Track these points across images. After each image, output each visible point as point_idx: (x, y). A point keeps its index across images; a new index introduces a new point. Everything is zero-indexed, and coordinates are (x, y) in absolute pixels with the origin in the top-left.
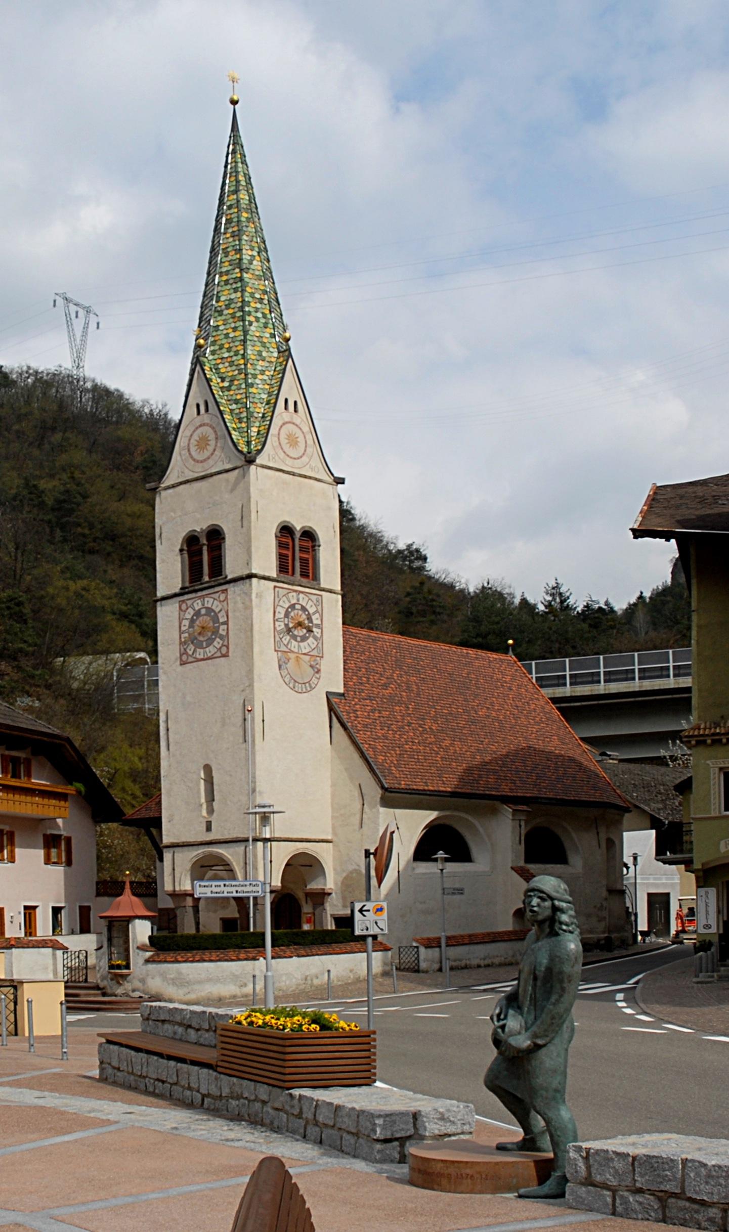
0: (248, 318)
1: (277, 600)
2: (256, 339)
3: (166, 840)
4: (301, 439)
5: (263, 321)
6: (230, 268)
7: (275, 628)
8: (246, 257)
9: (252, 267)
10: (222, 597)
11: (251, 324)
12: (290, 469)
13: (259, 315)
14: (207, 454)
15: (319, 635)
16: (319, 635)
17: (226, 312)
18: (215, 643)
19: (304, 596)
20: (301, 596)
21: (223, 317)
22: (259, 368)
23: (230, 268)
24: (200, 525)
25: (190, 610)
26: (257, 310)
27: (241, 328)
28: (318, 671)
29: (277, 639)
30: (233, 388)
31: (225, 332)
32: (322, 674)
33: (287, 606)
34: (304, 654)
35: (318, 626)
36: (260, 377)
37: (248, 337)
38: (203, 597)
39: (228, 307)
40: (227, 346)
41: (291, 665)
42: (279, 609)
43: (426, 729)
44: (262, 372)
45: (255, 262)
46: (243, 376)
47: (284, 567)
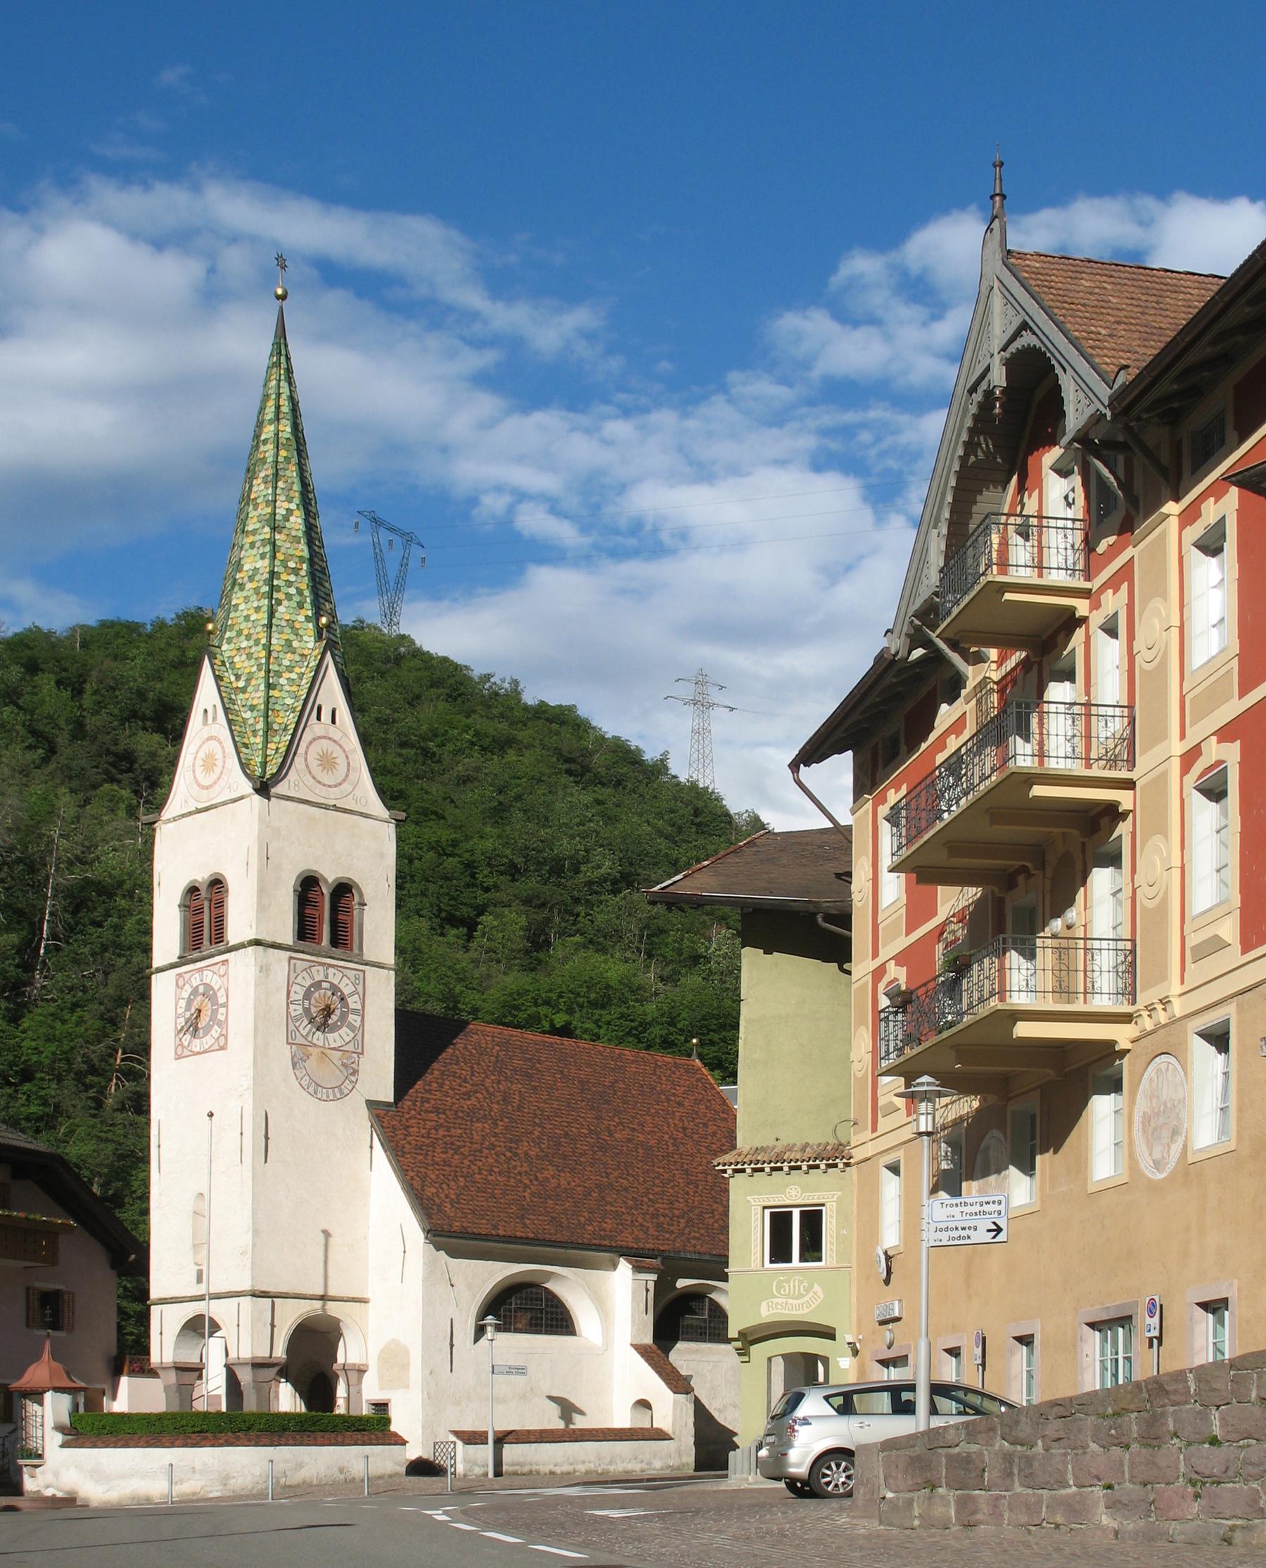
0: (275, 595)
1: (293, 975)
2: (284, 623)
3: (154, 1294)
4: (341, 761)
5: (297, 598)
6: (258, 525)
7: (288, 1013)
8: (281, 512)
9: (287, 524)
10: (223, 969)
11: (279, 602)
12: (321, 801)
13: (292, 591)
14: (214, 776)
15: (357, 1024)
16: (357, 1024)
17: (249, 586)
18: (213, 1032)
19: (339, 974)
20: (331, 971)
21: (245, 593)
22: (286, 663)
23: (258, 525)
24: (202, 876)
25: (187, 986)
26: (289, 584)
27: (265, 608)
28: (355, 1072)
29: (292, 1027)
30: (250, 689)
31: (245, 613)
32: (361, 1076)
33: (308, 983)
34: (334, 1049)
35: (356, 1012)
36: (286, 675)
37: (274, 621)
38: (201, 970)
39: (251, 579)
40: (246, 632)
41: (311, 1063)
42: (295, 988)
43: (516, 1154)
44: (290, 669)
45: (292, 519)
46: (262, 674)
47: (305, 930)
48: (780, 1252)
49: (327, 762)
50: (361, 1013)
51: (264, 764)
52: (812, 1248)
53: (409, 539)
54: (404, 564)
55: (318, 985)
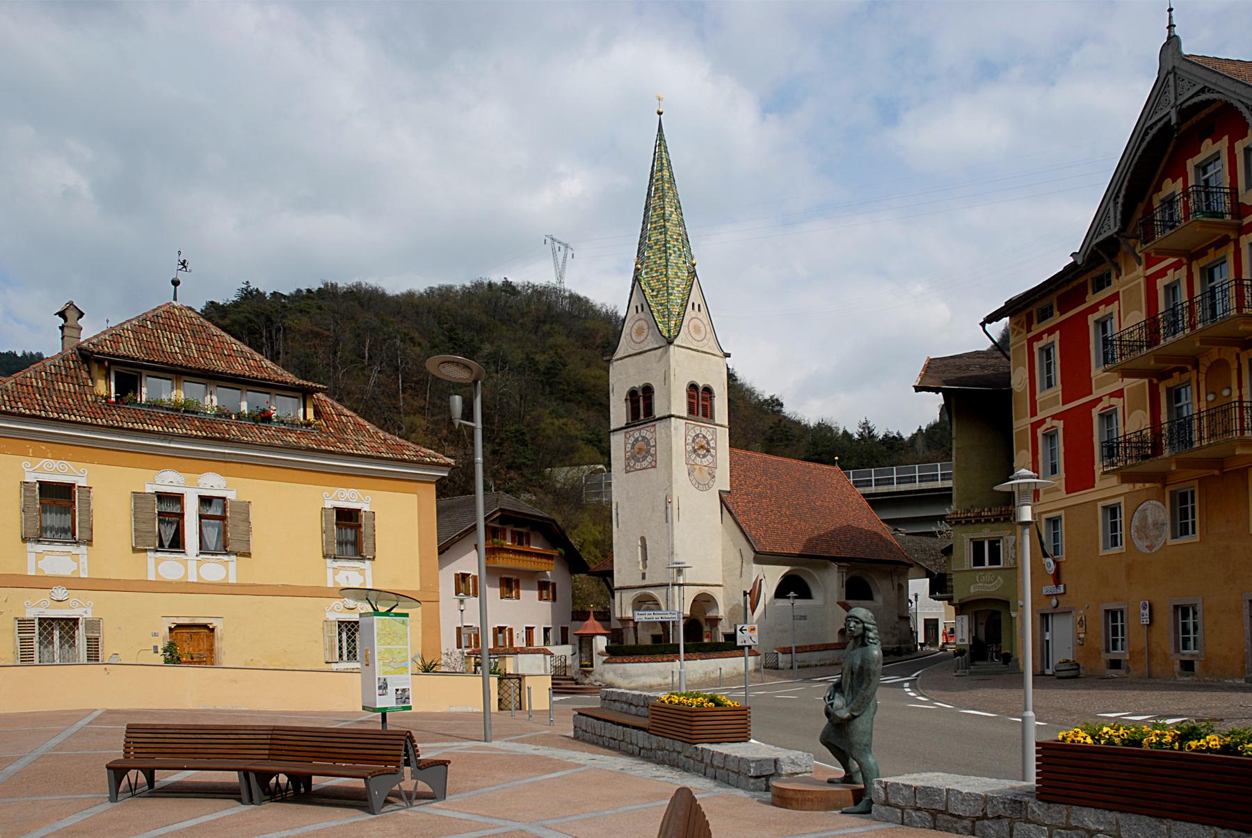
8: (667, 212)
14: (642, 338)
19: (704, 429)
24: (638, 384)
41: (696, 473)
47: (692, 410)
48: (978, 560)
49: (697, 330)
50: (714, 448)
51: (669, 331)
52: (995, 559)
53: (567, 246)
54: (565, 257)
55: (697, 436)
